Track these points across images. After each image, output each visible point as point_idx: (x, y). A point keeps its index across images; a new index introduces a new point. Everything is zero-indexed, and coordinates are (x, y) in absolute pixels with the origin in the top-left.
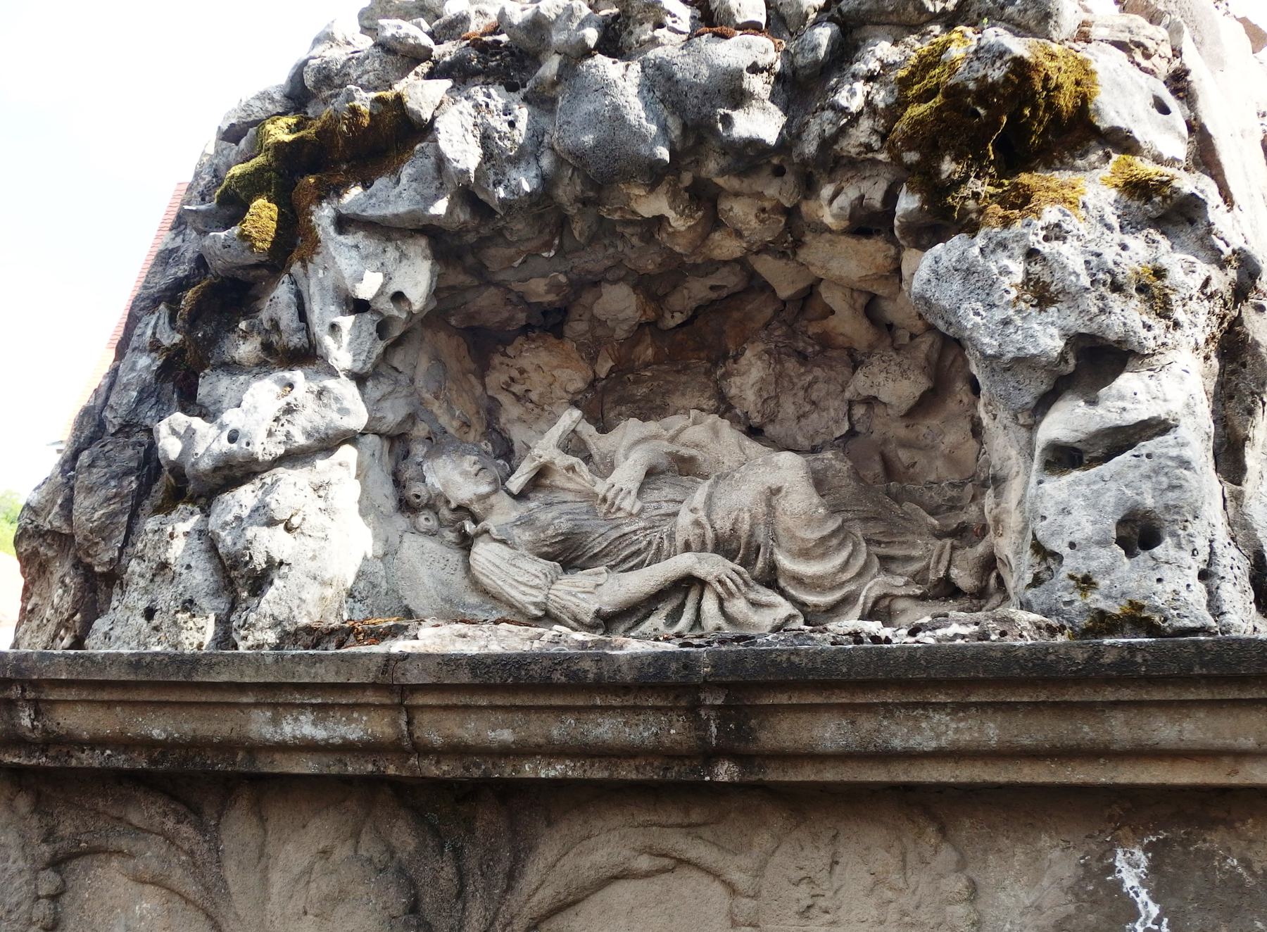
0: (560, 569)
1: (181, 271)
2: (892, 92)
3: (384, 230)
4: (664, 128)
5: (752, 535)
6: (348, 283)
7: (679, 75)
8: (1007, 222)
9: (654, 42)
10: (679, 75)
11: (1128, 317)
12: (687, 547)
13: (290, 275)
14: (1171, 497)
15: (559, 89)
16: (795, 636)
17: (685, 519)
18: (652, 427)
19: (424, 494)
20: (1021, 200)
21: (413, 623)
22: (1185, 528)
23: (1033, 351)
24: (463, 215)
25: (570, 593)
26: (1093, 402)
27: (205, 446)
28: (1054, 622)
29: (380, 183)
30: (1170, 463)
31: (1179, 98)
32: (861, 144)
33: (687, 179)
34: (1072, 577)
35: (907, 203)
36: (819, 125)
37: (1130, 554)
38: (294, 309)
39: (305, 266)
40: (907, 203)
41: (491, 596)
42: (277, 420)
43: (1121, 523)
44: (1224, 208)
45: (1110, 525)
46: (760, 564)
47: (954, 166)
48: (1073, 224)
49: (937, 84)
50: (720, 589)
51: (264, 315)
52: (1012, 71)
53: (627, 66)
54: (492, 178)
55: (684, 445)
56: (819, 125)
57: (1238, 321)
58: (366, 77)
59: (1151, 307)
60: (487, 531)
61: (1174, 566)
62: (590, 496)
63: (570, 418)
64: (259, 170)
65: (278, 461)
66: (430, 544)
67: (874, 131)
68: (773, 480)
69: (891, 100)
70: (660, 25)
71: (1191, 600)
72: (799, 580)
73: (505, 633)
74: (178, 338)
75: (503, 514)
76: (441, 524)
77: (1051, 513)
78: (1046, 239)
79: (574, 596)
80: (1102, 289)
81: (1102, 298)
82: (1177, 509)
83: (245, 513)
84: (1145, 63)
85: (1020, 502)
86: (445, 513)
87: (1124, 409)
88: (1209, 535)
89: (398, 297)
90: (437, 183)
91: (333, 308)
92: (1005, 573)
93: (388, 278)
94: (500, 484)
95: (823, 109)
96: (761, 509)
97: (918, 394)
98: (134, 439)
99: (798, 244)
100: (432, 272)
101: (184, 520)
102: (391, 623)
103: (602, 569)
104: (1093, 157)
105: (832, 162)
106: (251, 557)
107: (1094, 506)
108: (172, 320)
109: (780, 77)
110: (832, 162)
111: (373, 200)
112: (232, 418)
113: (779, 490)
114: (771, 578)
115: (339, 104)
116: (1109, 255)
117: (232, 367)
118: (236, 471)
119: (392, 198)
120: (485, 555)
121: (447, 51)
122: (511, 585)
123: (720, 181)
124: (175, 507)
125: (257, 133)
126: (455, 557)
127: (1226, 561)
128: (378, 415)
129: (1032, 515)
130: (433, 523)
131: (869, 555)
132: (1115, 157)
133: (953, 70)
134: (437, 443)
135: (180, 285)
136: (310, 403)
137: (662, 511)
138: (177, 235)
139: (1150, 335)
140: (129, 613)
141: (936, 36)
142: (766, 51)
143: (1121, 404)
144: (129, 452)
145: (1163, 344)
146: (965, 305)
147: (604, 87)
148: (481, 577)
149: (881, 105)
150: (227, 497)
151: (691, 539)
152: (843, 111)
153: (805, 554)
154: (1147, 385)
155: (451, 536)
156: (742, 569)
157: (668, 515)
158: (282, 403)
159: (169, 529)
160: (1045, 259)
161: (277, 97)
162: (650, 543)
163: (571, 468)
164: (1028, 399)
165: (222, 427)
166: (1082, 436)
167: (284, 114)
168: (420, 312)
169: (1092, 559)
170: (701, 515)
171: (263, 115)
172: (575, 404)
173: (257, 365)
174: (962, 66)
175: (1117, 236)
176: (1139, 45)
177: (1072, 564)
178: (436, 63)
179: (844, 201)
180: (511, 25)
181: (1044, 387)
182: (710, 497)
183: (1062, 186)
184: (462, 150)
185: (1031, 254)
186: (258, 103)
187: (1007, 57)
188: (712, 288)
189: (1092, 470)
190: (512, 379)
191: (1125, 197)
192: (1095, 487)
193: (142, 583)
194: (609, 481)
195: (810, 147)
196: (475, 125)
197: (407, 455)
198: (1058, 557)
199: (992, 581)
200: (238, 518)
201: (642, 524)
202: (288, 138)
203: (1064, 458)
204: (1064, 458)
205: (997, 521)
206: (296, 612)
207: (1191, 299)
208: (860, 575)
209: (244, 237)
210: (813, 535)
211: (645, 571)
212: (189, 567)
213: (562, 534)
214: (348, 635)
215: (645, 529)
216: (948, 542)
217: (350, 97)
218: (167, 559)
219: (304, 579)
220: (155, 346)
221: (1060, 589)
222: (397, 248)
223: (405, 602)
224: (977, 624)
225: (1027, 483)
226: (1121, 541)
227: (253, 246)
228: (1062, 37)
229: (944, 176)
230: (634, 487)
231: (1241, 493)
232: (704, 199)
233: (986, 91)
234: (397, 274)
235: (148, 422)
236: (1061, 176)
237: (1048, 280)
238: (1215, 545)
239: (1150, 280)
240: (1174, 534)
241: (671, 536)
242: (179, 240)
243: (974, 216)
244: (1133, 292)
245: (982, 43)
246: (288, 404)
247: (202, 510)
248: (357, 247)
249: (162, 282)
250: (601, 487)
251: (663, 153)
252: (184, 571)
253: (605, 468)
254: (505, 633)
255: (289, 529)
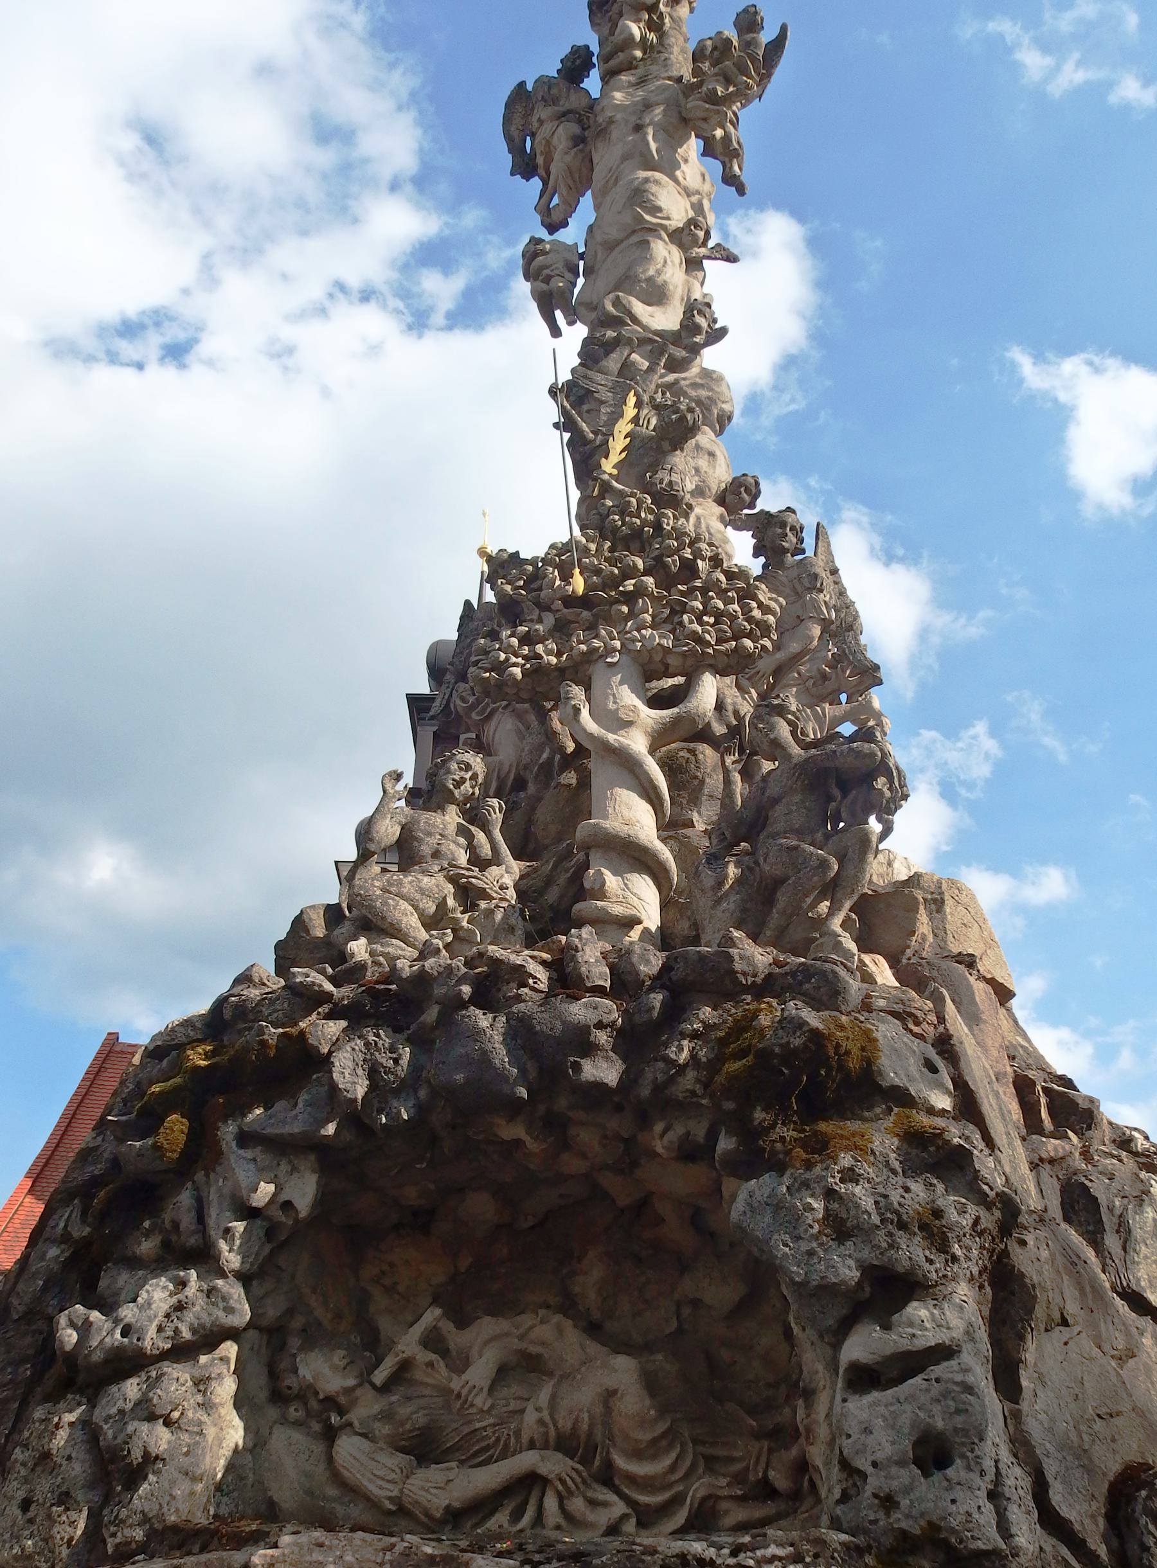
0: (415, 1463)
1: (97, 1169)
2: (713, 1049)
3: (280, 1149)
4: (523, 1071)
5: (590, 1434)
6: (244, 1193)
7: (538, 1028)
8: (809, 1165)
9: (518, 998)
10: (538, 1028)
11: (912, 1251)
12: (532, 1445)
13: (194, 1182)
14: (959, 1421)
15: (437, 1032)
16: (628, 1558)
17: (531, 1417)
18: (504, 1325)
19: (295, 1385)
20: (820, 1147)
21: (274, 1527)
22: (972, 1451)
23: (834, 1280)
24: (348, 1136)
25: (423, 1488)
26: (887, 1327)
27: (99, 1338)
28: (860, 1541)
29: (280, 1105)
30: (955, 1388)
31: (944, 1058)
32: (687, 1090)
33: (542, 1108)
34: (875, 1496)
35: (725, 1144)
36: (653, 1073)
37: (926, 1474)
38: (193, 1213)
39: (207, 1176)
40: (725, 1144)
41: (351, 1491)
42: (167, 1316)
43: (917, 1444)
44: (987, 1151)
45: (907, 1444)
46: (597, 1463)
47: (764, 1115)
48: (866, 1169)
49: (750, 1045)
50: (560, 1488)
51: (167, 1216)
52: (810, 1040)
53: (495, 1017)
54: (376, 1105)
55: (532, 1342)
56: (653, 1073)
57: (1005, 1253)
58: (275, 1015)
59: (932, 1243)
60: (350, 1424)
61: (965, 1488)
62: (446, 1392)
63: (431, 1315)
64: (176, 1089)
65: (165, 1356)
66: (297, 1436)
67: (698, 1080)
68: (610, 1382)
69: (712, 1056)
70: (524, 985)
71: (982, 1522)
72: (632, 1479)
73: (359, 1543)
74: (87, 1230)
75: (367, 1407)
76: (308, 1413)
77: (855, 1431)
78: (842, 1180)
79: (427, 1491)
80: (890, 1227)
81: (890, 1234)
82: (965, 1432)
83: (129, 1406)
84: (916, 1029)
85: (827, 1415)
86: (313, 1404)
87: (914, 1335)
88: (993, 1455)
89: (288, 1205)
90: (328, 1109)
91: (228, 1214)
92: (816, 1477)
93: (279, 1189)
94: (365, 1378)
95: (656, 1060)
96: (599, 1410)
97: (737, 1299)
98: (34, 1327)
99: (635, 1164)
100: (318, 1183)
101: (70, 1411)
102: (254, 1527)
103: (454, 1464)
104: (878, 1110)
105: (663, 1103)
106: (129, 1452)
107: (893, 1427)
108: (84, 1214)
109: (620, 1031)
110: (663, 1103)
111: (272, 1121)
112: (128, 1313)
113: (615, 1392)
114: (607, 1477)
115: (250, 1037)
116: (895, 1197)
117: (134, 1263)
118: (128, 1362)
119: (289, 1120)
120: (348, 1447)
121: (344, 993)
122: (370, 1480)
123: (570, 1114)
124: (64, 1397)
125: (178, 1055)
126: (319, 1448)
127: (1010, 1482)
128: (260, 1311)
129: (838, 1433)
130: (301, 1414)
131: (695, 1455)
132: (896, 1110)
133: (763, 1036)
134: (313, 1338)
135: (95, 1183)
136: (201, 1301)
137: (511, 1408)
138: (98, 1135)
139: (932, 1268)
140: (6, 1503)
141: (748, 1004)
142: (610, 1012)
143: (910, 1330)
144: (29, 1339)
145: (945, 1276)
146: (776, 1236)
147: (477, 1034)
148: (342, 1470)
149: (704, 1060)
150: (114, 1389)
151: (536, 1437)
152: (673, 1063)
153: (638, 1454)
154: (932, 1314)
155: (316, 1427)
156: (580, 1467)
157: (515, 1412)
158: (174, 1300)
159: (56, 1419)
160: (841, 1198)
161: (199, 1025)
162: (498, 1439)
163: (430, 1364)
164: (831, 1322)
165: (117, 1321)
166: (879, 1359)
167: (200, 1041)
168: (305, 1218)
169: (893, 1478)
170: (545, 1415)
171: (184, 1040)
172: (436, 1301)
173: (156, 1261)
174: (769, 1034)
175: (900, 1180)
176: (910, 1015)
177: (875, 1482)
178: (336, 1004)
179: (671, 1136)
180: (401, 978)
181: (844, 1311)
182: (553, 1397)
183: (853, 1135)
184: (353, 1082)
185: (830, 1194)
186: (182, 1029)
187: (805, 1028)
188: (561, 1196)
189: (889, 1392)
190: (383, 1273)
191: (905, 1146)
192: (892, 1409)
193: (23, 1472)
194: (465, 1377)
195: (645, 1092)
196: (365, 1060)
197: (282, 1346)
198: (864, 1476)
199: (806, 1484)
200: (121, 1412)
201: (492, 1421)
202: (204, 1063)
203: (865, 1378)
204: (865, 1378)
205: (808, 1430)
206: (165, 1509)
207: (965, 1236)
208: (687, 1476)
209: (157, 1147)
210: (645, 1436)
211: (494, 1467)
212: (69, 1458)
213: (419, 1429)
214: (213, 1538)
215: (494, 1425)
216: (766, 1444)
217: (261, 1032)
218: (50, 1450)
219: (176, 1474)
220: (66, 1238)
221: (866, 1508)
222: (290, 1162)
223: (270, 1494)
224: (792, 1545)
225: (833, 1398)
226: (918, 1462)
227: (164, 1155)
228: (849, 1009)
229: (756, 1123)
230: (486, 1384)
231: (1019, 1411)
232: (555, 1127)
233: (789, 1054)
234: (287, 1186)
235: (50, 1310)
236: (853, 1126)
237: (845, 1216)
238: (1001, 1465)
239: (928, 1219)
240: (963, 1456)
241: (518, 1433)
242: (100, 1139)
243: (781, 1156)
244: (916, 1230)
245: (786, 1014)
246: (179, 1302)
247: (89, 1401)
248: (254, 1160)
249: (81, 1177)
250: (456, 1384)
251: (523, 1092)
252: (64, 1462)
253: (460, 1363)
254: (359, 1543)
255: (168, 1423)
